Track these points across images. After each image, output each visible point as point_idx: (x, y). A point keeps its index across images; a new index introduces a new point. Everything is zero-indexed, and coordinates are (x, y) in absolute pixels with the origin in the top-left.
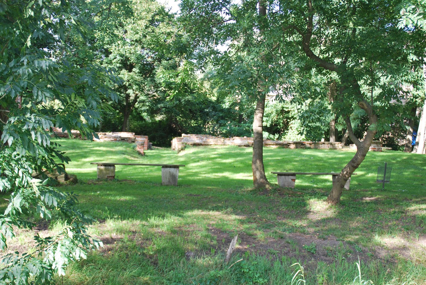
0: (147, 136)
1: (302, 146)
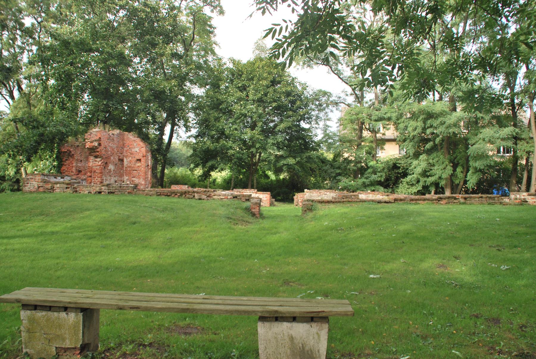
0: (269, 193)
1: (455, 201)
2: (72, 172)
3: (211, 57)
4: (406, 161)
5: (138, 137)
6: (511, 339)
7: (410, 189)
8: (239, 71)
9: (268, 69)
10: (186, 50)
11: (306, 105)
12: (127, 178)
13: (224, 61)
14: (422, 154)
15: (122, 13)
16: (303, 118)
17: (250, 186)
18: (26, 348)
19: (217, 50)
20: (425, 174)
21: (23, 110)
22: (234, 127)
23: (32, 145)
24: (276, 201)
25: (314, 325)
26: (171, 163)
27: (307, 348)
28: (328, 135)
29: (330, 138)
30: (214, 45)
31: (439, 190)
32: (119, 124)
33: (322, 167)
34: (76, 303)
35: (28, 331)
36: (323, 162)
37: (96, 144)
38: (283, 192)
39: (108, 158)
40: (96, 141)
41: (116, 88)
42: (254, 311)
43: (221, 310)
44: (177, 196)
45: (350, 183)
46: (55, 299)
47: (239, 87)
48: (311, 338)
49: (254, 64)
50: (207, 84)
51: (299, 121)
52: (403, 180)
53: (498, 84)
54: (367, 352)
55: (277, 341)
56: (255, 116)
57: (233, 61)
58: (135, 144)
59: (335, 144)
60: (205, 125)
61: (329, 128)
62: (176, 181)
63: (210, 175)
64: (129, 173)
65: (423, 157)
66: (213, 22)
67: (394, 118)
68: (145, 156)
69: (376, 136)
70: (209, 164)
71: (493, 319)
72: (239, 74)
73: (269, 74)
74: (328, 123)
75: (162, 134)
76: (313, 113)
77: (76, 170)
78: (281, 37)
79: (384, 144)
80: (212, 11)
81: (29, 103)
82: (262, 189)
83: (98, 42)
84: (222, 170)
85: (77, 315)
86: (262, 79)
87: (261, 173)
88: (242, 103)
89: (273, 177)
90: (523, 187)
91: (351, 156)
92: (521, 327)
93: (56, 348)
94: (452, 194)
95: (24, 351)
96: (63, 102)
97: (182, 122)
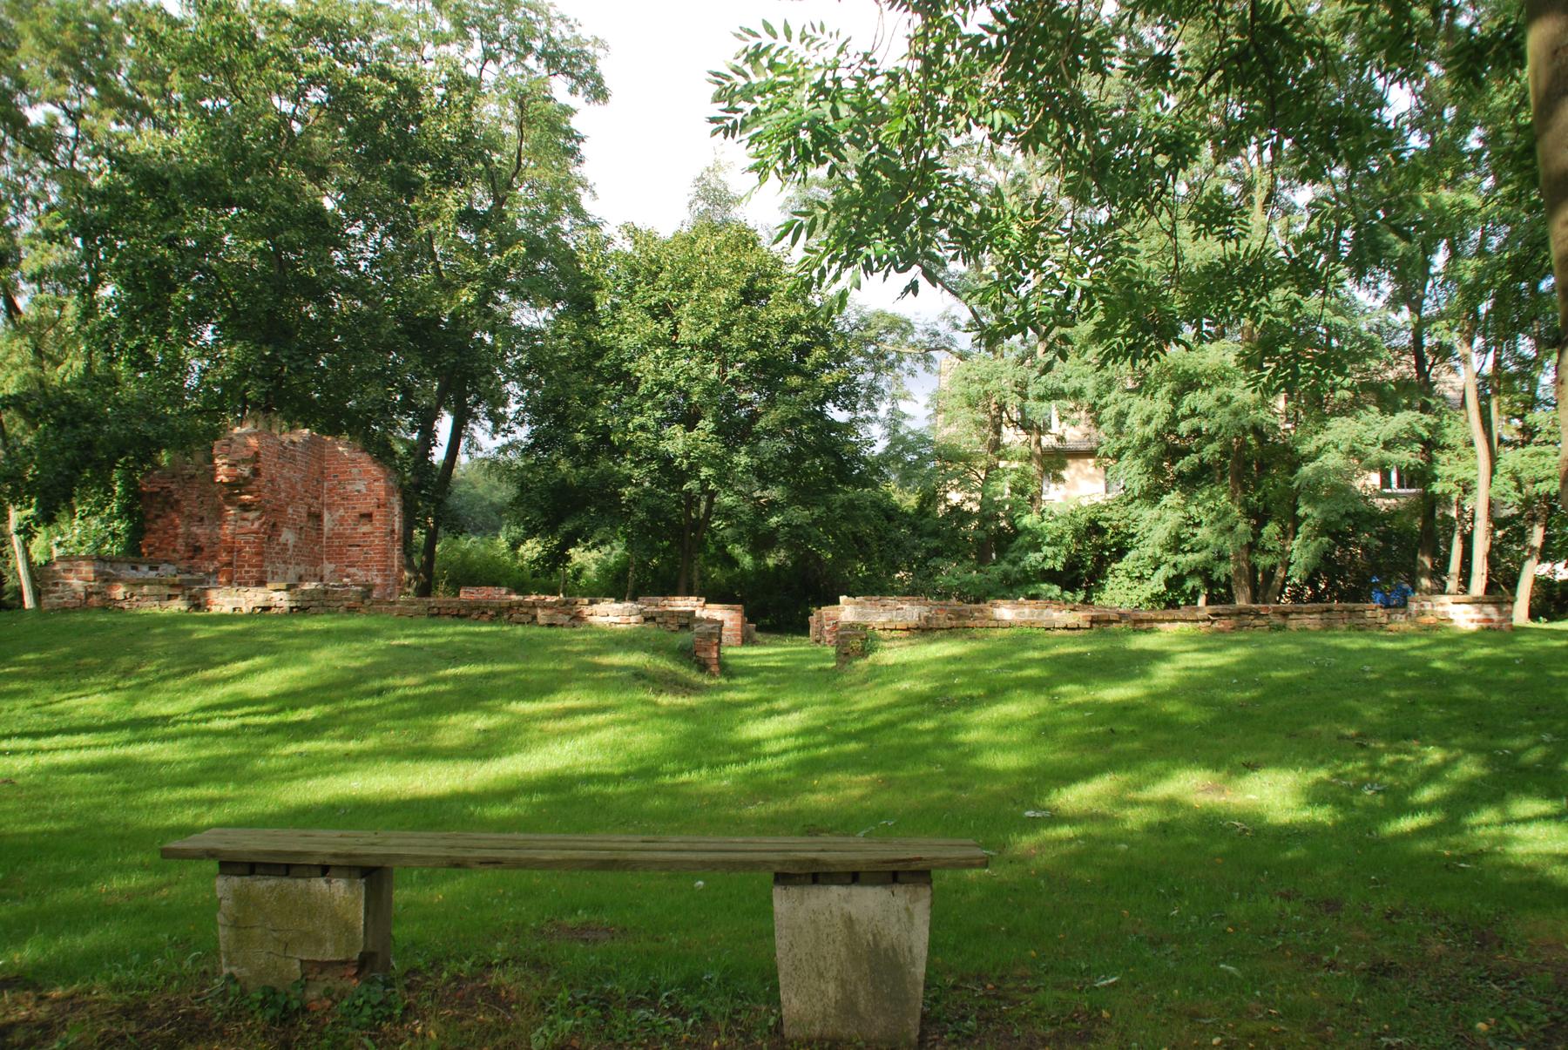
0: (739, 607)
1: (1257, 622)
2: (174, 551)
3: (567, 221)
4: (1123, 512)
5: (363, 451)
6: (1360, 940)
7: (1136, 591)
8: (652, 261)
9: (733, 257)
10: (500, 201)
11: (841, 357)
12: (332, 566)
13: (607, 231)
14: (1168, 493)
15: (316, 95)
16: (831, 394)
17: (683, 588)
18: (230, 964)
19: (586, 203)
20: (1176, 544)
21: (22, 372)
22: (638, 420)
23: (59, 474)
24: (758, 629)
25: (899, 889)
26: (455, 524)
27: (884, 944)
28: (902, 440)
29: (910, 448)
30: (580, 190)
31: (1220, 593)
32: (302, 412)
33: (887, 531)
34: (350, 856)
35: (236, 924)
36: (890, 519)
37: (246, 471)
38: (780, 605)
39: (279, 510)
40: (244, 461)
41: (320, 315)
42: (765, 862)
43: (691, 862)
44: (485, 618)
45: (968, 577)
46: (298, 848)
47: (649, 309)
48: (894, 919)
49: (694, 242)
50: (555, 299)
51: (822, 402)
52: (1120, 565)
53: (1377, 296)
54: (1019, 972)
55: (817, 930)
56: (698, 389)
57: (632, 232)
58: (355, 470)
59: (922, 466)
60: (552, 414)
61: (906, 422)
62: (468, 575)
63: (568, 558)
64: (337, 554)
65: (1172, 498)
66: (575, 123)
67: (1090, 394)
68: (384, 505)
69: (1038, 442)
70: (568, 526)
71: (1327, 903)
72: (649, 271)
73: (736, 270)
74: (903, 406)
75: (428, 436)
76: (861, 379)
77: (187, 545)
78: (813, 242)
79: (1063, 466)
80: (573, 91)
81: (38, 351)
82: (715, 596)
83: (248, 180)
84: (603, 542)
85: (350, 885)
86: (717, 285)
87: (712, 549)
88: (659, 352)
89: (747, 561)
90: (1452, 584)
91: (970, 500)
92: (1388, 917)
93: (302, 961)
94: (1255, 602)
95: (226, 971)
96: (141, 349)
97: (481, 410)
